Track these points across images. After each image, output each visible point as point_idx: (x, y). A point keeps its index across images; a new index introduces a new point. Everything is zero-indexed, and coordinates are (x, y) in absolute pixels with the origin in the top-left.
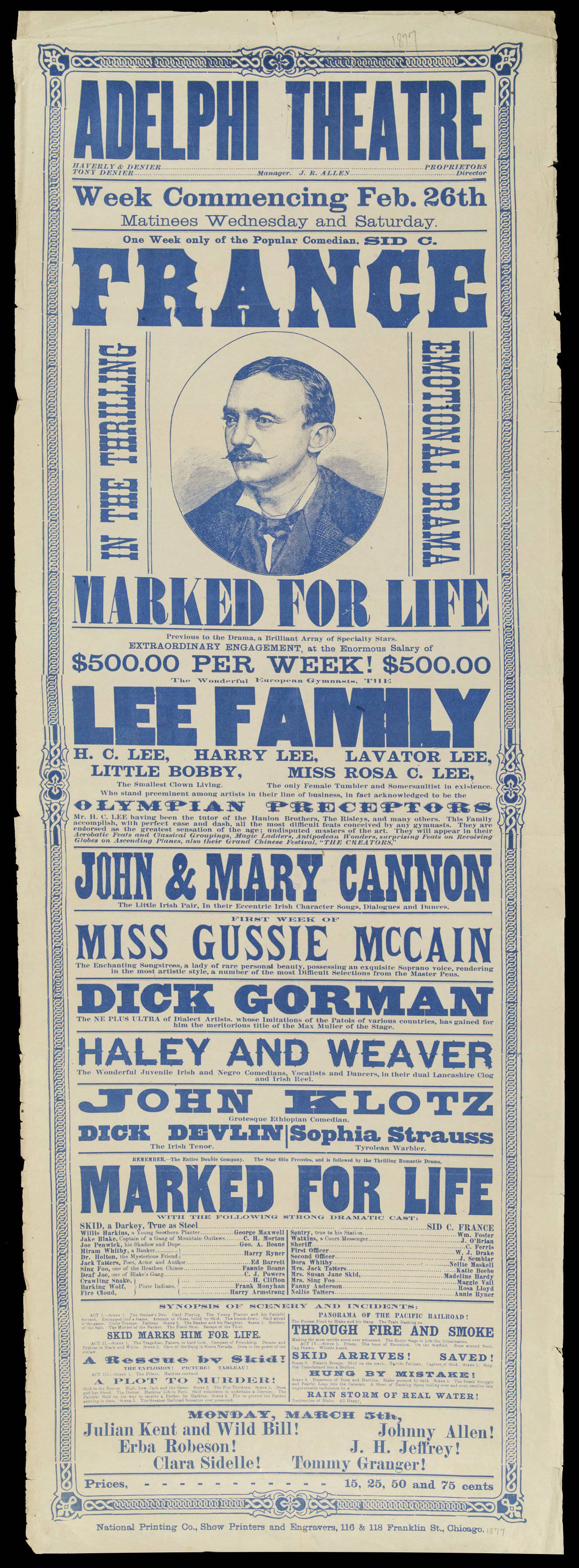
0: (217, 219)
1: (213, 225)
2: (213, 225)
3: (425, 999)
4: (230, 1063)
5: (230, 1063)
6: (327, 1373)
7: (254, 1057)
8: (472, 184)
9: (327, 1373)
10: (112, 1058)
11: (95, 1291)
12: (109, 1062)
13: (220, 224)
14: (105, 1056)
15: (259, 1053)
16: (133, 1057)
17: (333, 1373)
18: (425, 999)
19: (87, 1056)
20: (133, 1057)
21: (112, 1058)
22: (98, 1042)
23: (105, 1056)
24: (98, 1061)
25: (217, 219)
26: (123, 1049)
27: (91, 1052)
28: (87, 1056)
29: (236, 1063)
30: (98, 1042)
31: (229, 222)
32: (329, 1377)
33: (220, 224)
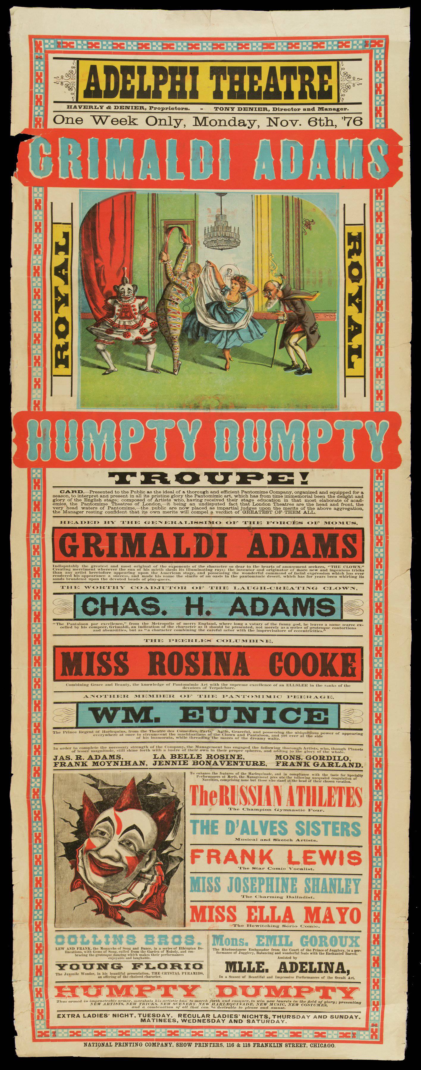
0: (101, 118)
1: (97, 123)
2: (97, 123)
3: (159, 546)
4: (231, 614)
5: (231, 614)
6: (88, 967)
7: (290, 610)
8: (326, 116)
9: (88, 967)
10: (125, 610)
11: (188, 737)
12: (123, 613)
13: (104, 123)
14: (120, 609)
15: (295, 608)
16: (249, 610)
17: (96, 967)
18: (159, 546)
19: (107, 610)
20: (249, 610)
21: (275, 610)
22: (115, 600)
23: (120, 609)
24: (115, 613)
25: (101, 118)
26: (134, 605)
27: (109, 606)
28: (107, 610)
29: (127, 613)
30: (115, 600)
31: (112, 121)
32: (91, 971)
33: (104, 123)
